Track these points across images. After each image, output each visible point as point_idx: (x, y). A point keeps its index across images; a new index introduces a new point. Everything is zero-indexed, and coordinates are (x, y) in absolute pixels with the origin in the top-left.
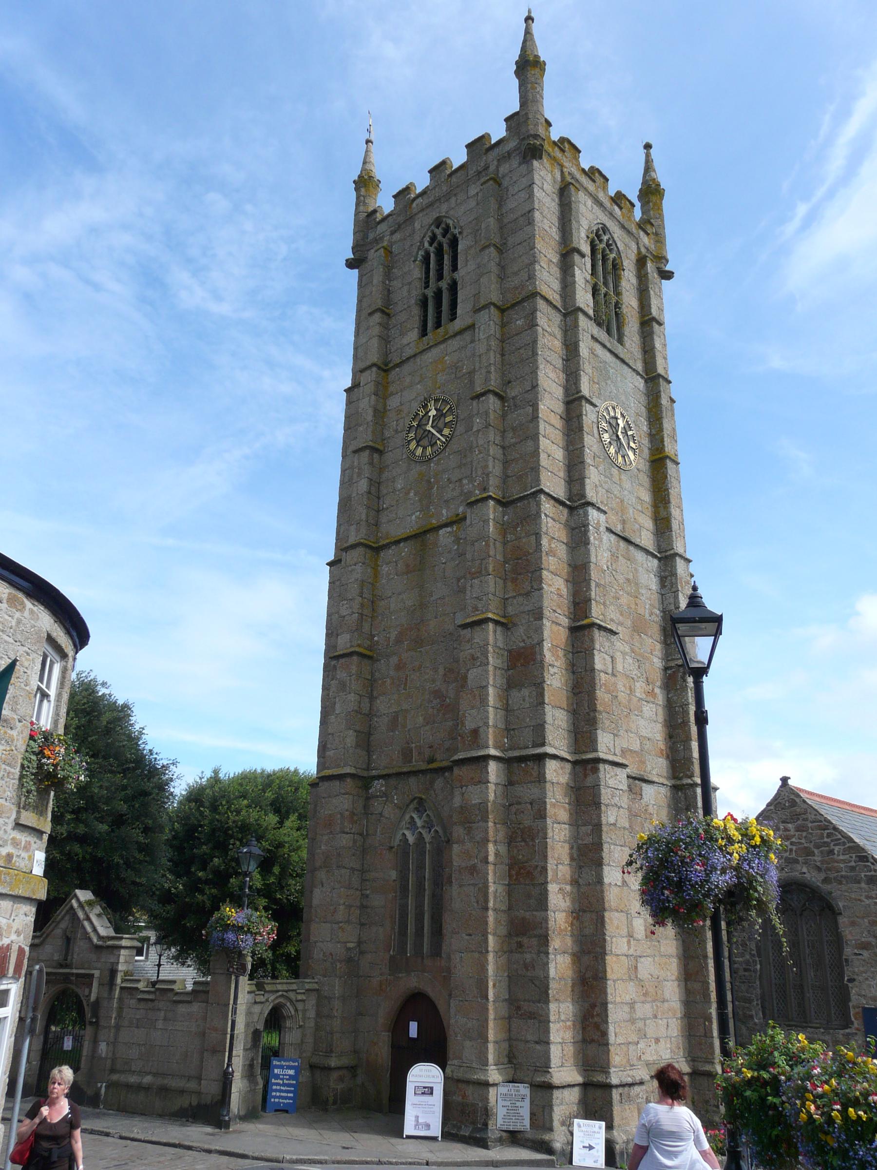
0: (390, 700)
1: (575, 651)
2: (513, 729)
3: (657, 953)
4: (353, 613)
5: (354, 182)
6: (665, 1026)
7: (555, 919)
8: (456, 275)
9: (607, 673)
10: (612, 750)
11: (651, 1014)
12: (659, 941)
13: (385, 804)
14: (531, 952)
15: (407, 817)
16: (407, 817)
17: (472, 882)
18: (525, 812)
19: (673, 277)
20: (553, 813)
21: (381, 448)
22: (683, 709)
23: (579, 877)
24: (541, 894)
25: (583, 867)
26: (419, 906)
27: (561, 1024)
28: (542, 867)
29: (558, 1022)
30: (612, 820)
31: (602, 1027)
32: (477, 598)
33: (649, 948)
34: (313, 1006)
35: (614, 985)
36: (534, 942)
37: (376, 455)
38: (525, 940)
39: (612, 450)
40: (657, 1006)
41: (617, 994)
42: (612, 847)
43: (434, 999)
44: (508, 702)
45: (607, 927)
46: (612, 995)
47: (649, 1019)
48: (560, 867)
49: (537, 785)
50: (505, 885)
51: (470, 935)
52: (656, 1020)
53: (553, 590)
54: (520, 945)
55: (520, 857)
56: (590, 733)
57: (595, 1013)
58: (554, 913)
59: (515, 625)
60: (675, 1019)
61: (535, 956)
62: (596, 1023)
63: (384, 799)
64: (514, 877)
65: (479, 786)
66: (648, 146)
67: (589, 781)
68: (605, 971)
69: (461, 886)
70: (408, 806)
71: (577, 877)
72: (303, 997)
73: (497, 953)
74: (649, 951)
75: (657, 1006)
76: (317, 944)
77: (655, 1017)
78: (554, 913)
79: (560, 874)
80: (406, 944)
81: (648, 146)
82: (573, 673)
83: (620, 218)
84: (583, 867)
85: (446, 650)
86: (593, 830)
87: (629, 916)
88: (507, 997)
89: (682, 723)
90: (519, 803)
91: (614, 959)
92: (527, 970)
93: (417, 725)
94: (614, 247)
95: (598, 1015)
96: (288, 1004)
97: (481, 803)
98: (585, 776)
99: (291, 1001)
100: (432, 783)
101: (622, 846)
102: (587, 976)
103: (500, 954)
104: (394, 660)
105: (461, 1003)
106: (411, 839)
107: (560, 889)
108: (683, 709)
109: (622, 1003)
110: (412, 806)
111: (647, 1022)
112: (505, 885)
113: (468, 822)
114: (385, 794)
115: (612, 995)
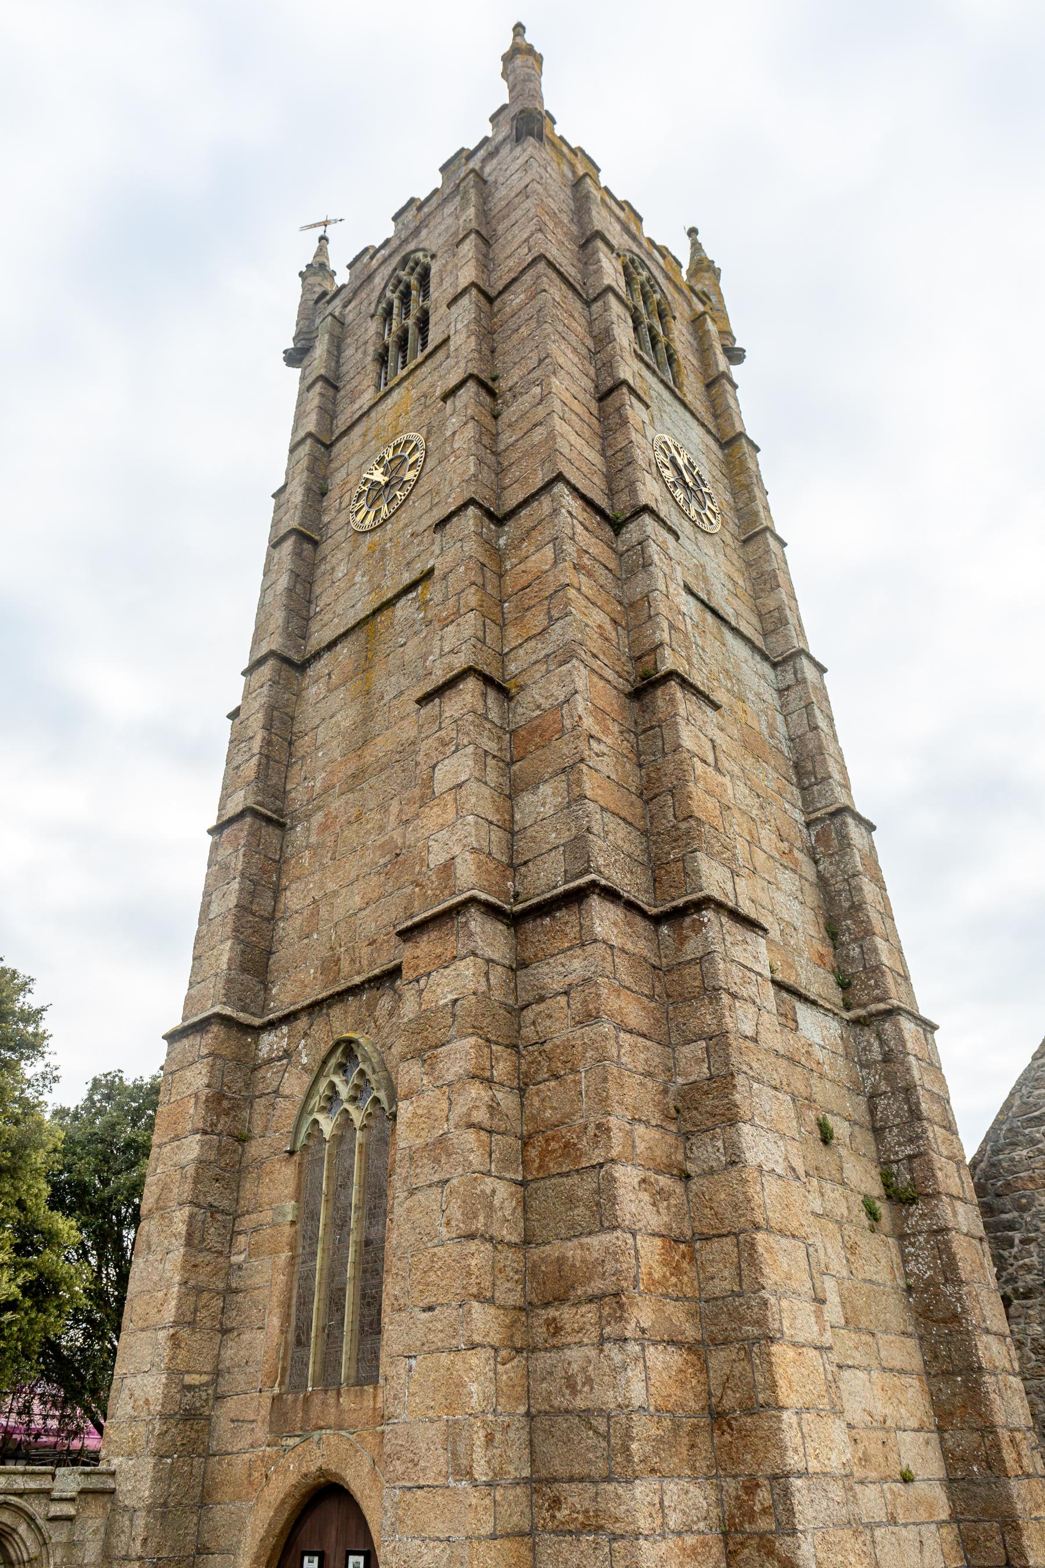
0: (307, 885)
1: (640, 728)
2: (525, 863)
3: (874, 1363)
4: (253, 755)
5: (301, 274)
6: (917, 1544)
7: (637, 1251)
8: (427, 303)
9: (705, 762)
10: (732, 897)
11: (882, 1513)
12: (873, 1335)
13: (285, 1071)
14: (580, 1344)
15: (323, 1086)
16: (323, 1086)
17: (436, 1178)
18: (556, 1015)
19: (745, 357)
20: (616, 1006)
21: (317, 538)
22: (849, 885)
23: (687, 1158)
24: (598, 1191)
25: (693, 1133)
26: (335, 1272)
27: (672, 1541)
28: (599, 1126)
29: (663, 1536)
30: (748, 1029)
31: (782, 1545)
32: (452, 651)
33: (857, 1348)
34: (95, 1532)
35: (799, 1424)
36: (588, 1313)
37: (307, 546)
38: (566, 1314)
40: (892, 1492)
41: (810, 1451)
42: (755, 1085)
43: (358, 1496)
44: (513, 816)
45: (766, 1271)
46: (796, 1451)
47: (879, 1525)
48: (640, 1129)
49: (579, 951)
50: (515, 1182)
51: (431, 1309)
52: (896, 1529)
53: (590, 623)
54: (555, 1328)
55: (548, 1113)
56: (684, 861)
57: (757, 1508)
58: (634, 1236)
59: (521, 688)
60: (933, 1527)
61: (593, 1353)
62: (762, 1535)
63: (285, 1061)
64: (536, 1165)
65: (453, 967)
66: (693, 232)
67: (692, 948)
68: (773, 1386)
69: (412, 1192)
70: (325, 1062)
71: (680, 1157)
72: (69, 1510)
73: (496, 1350)
74: (856, 1354)
75: (892, 1492)
76: (126, 1381)
77: (893, 1521)
78: (634, 1236)
79: (641, 1147)
80: (307, 1365)
81: (693, 232)
82: (640, 766)
83: (663, 265)
84: (693, 1133)
85: (403, 771)
86: (707, 1049)
87: (811, 1250)
88: (526, 1473)
89: (851, 908)
90: (542, 999)
91: (791, 1353)
92: (574, 1392)
93: (351, 912)
94: (657, 288)
95: (764, 1511)
96: (22, 1529)
97: (456, 1001)
98: (682, 940)
99: (31, 1519)
100: (371, 1007)
101: (775, 1088)
102: (727, 1403)
103: (504, 1353)
104: (318, 818)
105: (408, 1496)
106: (327, 1126)
107: (644, 1181)
108: (849, 885)
109: (825, 1474)
110: (333, 1062)
111: (878, 1533)
112: (515, 1182)
113: (431, 1047)
114: (287, 1054)
115: (796, 1451)
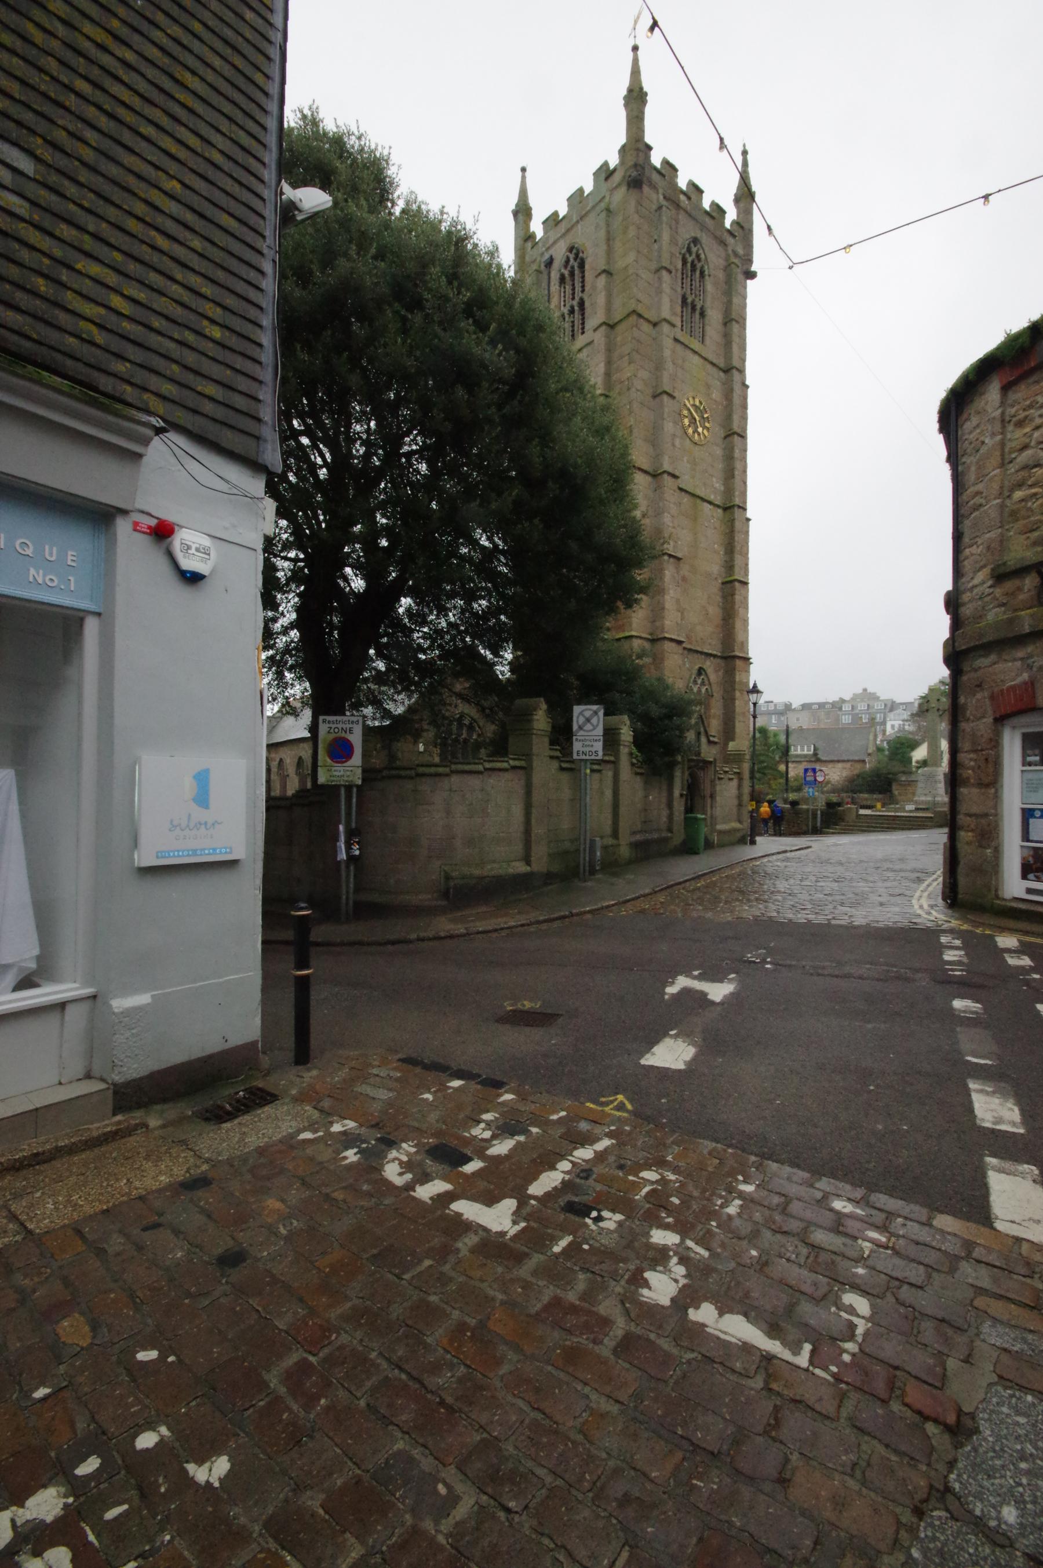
39: (690, 431)
66: (523, 170)
81: (523, 170)
